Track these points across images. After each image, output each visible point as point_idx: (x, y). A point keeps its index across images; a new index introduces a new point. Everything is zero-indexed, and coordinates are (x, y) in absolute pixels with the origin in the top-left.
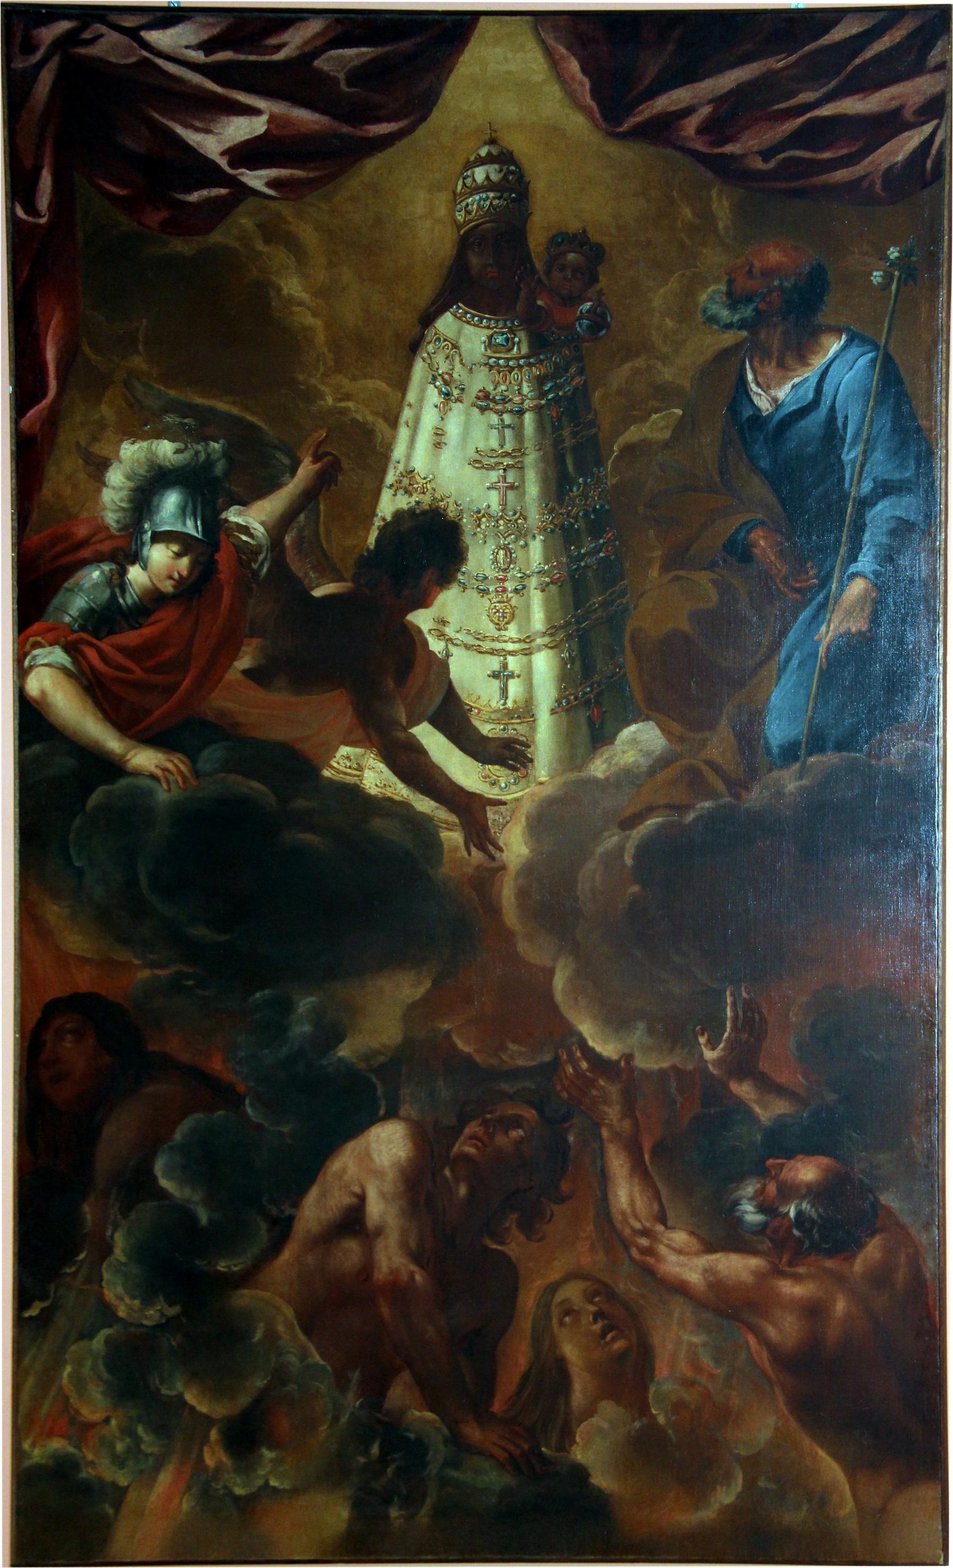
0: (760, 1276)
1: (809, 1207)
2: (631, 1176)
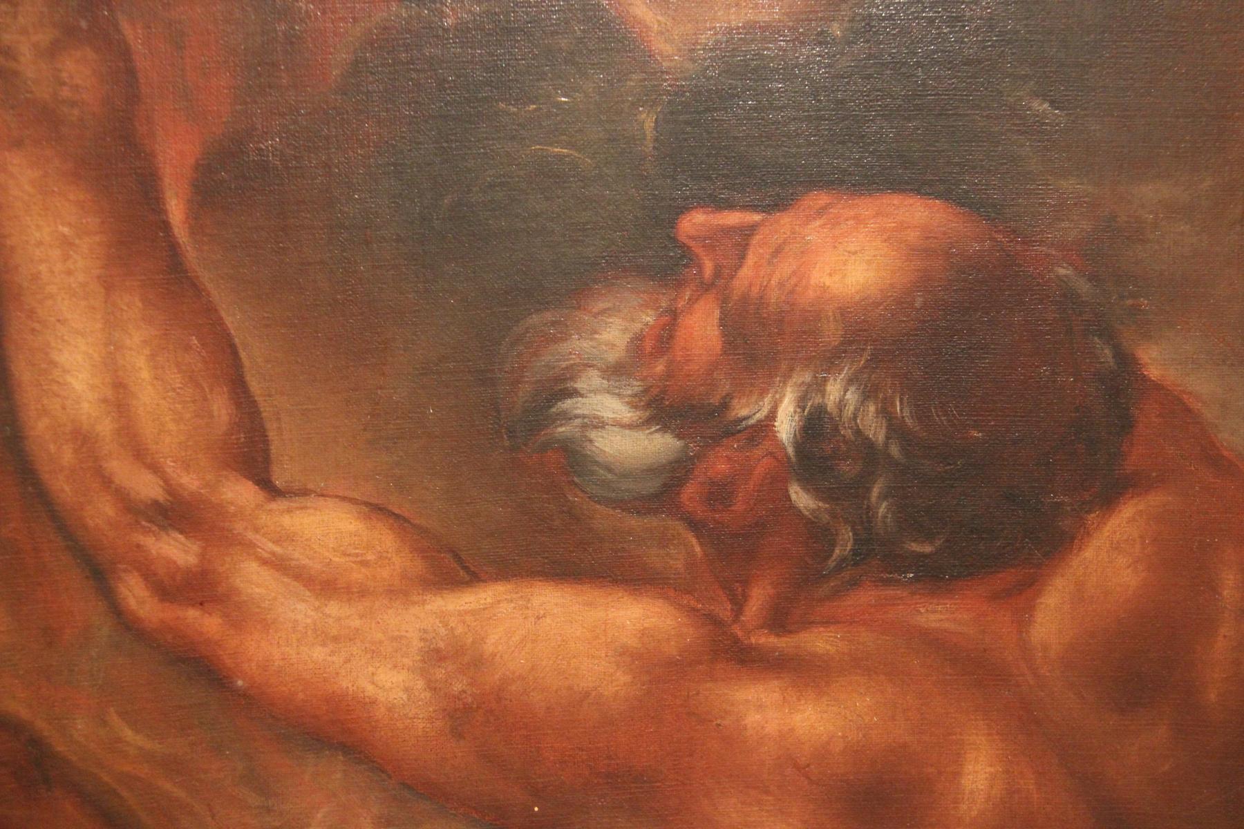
0: (661, 672)
1: (852, 397)
2: (109, 287)
